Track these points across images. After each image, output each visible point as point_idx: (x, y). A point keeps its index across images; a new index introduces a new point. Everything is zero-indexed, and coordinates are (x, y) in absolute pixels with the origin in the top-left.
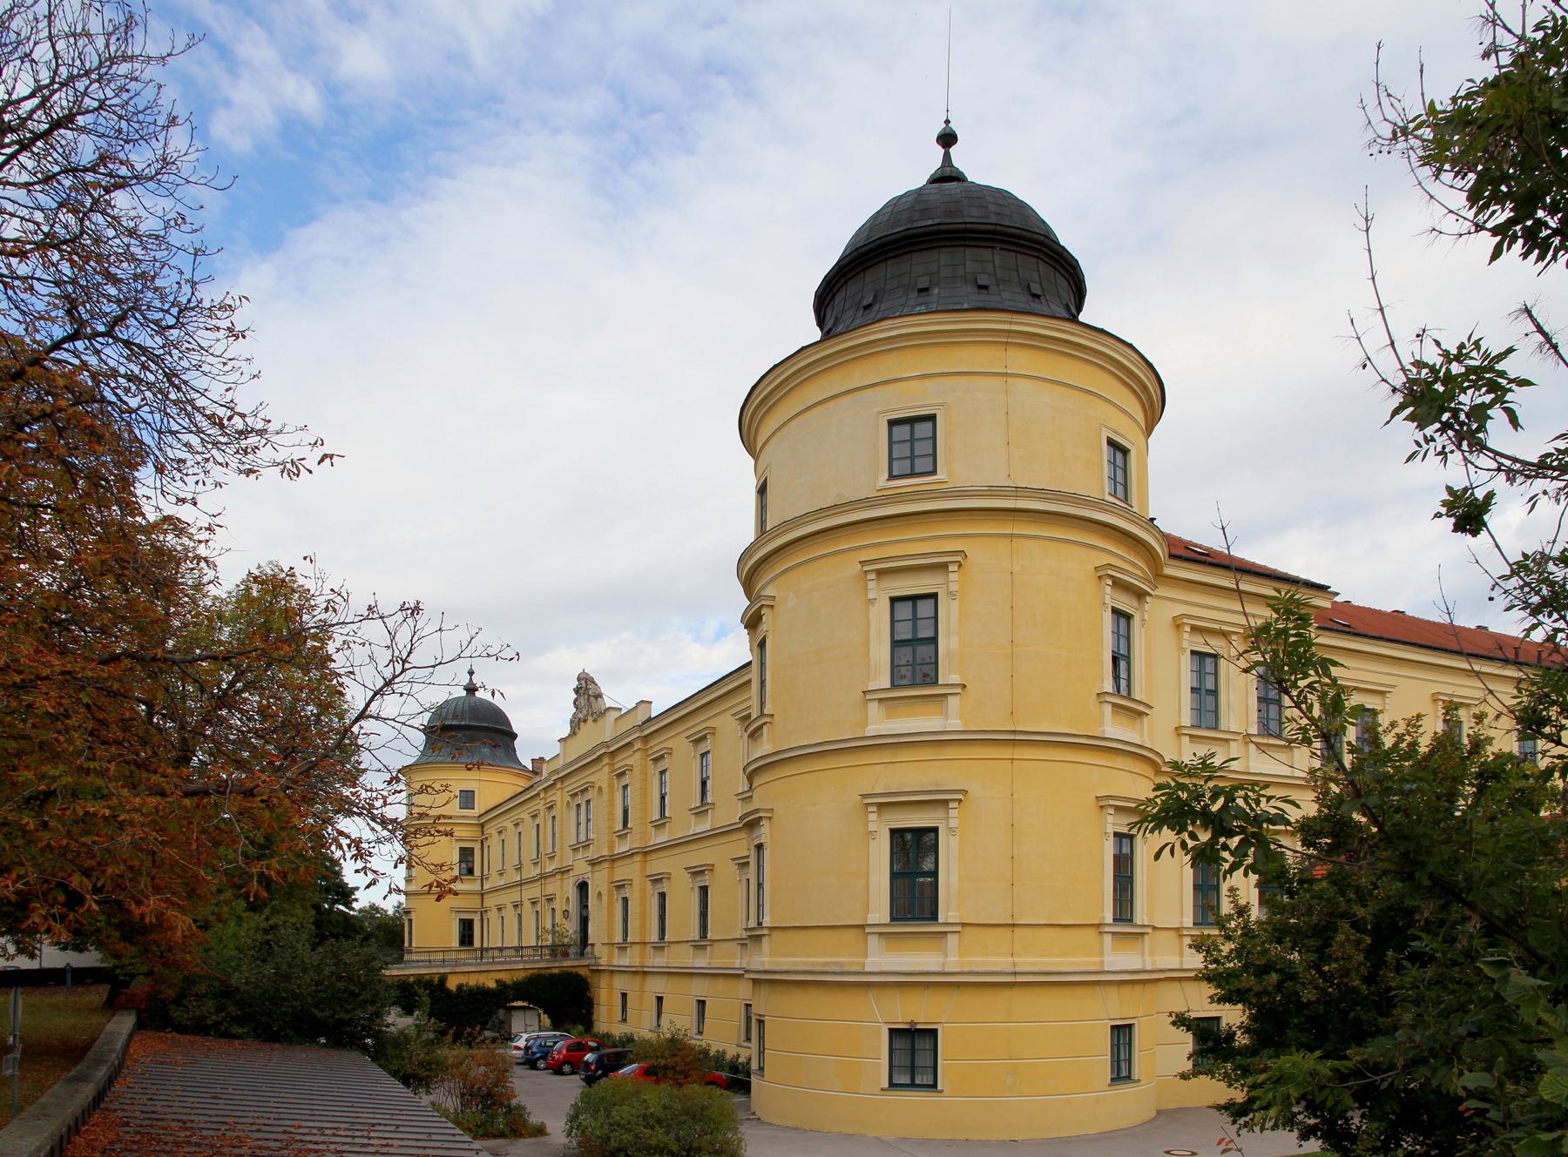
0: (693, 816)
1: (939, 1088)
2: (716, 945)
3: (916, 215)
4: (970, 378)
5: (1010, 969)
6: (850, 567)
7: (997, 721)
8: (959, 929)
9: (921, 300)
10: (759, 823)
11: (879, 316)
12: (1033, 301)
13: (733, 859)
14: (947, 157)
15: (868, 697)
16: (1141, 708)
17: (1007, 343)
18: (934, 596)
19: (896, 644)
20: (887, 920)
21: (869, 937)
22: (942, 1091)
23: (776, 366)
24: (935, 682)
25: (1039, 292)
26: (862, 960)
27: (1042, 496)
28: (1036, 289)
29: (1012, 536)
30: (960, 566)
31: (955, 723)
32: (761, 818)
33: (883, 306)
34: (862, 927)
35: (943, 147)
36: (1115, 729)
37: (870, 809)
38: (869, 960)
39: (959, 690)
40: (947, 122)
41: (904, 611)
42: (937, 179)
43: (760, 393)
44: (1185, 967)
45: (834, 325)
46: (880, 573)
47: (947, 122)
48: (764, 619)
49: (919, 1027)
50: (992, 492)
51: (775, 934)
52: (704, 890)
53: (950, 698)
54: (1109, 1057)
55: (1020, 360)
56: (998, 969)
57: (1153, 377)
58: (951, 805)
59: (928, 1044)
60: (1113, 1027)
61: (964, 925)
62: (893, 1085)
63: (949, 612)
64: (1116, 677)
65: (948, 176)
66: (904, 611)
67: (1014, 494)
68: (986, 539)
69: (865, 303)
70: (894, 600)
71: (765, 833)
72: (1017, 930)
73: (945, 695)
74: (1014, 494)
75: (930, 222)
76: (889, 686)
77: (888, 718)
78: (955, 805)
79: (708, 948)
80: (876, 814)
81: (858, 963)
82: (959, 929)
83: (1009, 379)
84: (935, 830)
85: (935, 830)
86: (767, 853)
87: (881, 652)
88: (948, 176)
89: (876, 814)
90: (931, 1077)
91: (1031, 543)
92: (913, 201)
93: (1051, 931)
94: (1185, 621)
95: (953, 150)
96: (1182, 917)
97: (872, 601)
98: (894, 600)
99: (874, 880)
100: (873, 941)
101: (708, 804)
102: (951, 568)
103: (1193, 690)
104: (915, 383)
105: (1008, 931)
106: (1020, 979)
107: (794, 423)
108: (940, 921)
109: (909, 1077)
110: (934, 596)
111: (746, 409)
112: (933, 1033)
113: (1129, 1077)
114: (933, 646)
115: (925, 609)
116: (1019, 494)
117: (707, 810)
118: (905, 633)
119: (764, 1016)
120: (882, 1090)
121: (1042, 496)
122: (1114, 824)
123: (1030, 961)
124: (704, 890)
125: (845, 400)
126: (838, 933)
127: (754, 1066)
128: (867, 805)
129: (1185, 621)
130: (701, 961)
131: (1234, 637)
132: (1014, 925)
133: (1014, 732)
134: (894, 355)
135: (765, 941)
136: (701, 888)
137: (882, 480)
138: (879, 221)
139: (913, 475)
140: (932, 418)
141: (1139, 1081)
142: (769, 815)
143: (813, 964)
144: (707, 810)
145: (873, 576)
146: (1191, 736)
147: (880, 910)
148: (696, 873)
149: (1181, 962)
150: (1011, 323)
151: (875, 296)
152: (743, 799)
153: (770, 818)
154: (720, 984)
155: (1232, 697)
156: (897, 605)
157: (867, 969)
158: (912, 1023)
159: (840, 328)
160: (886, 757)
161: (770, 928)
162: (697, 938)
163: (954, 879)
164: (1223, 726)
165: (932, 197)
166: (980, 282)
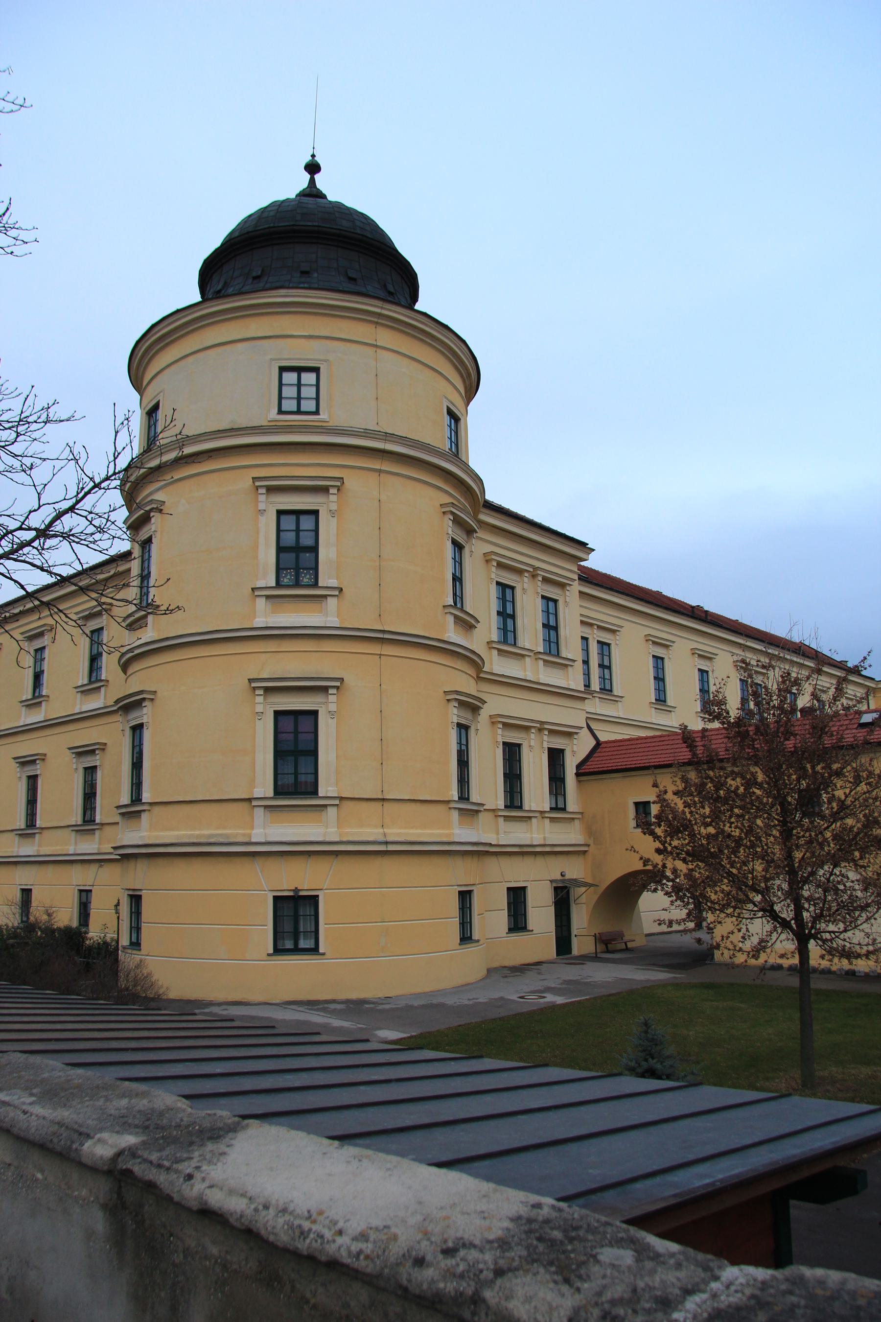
0: (24, 708)
1: (321, 951)
2: (45, 832)
3: (298, 217)
4: (348, 344)
5: (381, 839)
6: (244, 481)
7: (367, 621)
8: (337, 802)
9: (303, 279)
10: (141, 704)
11: (268, 286)
12: (390, 297)
13: (70, 749)
14: (312, 182)
15: (257, 593)
16: (473, 622)
17: (377, 323)
18: (316, 513)
19: (281, 550)
20: (270, 793)
21: (256, 809)
22: (324, 954)
23: (178, 311)
24: (315, 585)
25: (392, 290)
26: (248, 831)
27: (404, 442)
28: (391, 288)
29: (380, 471)
30: (338, 490)
31: (333, 620)
32: (144, 699)
33: (271, 279)
34: (249, 800)
35: (309, 173)
36: (453, 634)
37: (257, 692)
38: (255, 831)
39: (337, 593)
40: (313, 156)
41: (289, 523)
42: (302, 194)
43: (159, 331)
44: (500, 843)
45: (223, 287)
46: (271, 490)
47: (313, 156)
48: (153, 520)
49: (302, 893)
50: (367, 433)
51: (157, 809)
52: (33, 780)
53: (329, 598)
54: (458, 919)
55: (385, 337)
56: (371, 839)
57: (473, 365)
58: (331, 691)
59: (309, 911)
60: (460, 892)
61: (341, 799)
62: (278, 950)
63: (328, 528)
64: (455, 595)
65: (312, 193)
66: (289, 523)
67: (384, 438)
68: (357, 471)
69: (254, 274)
70: (280, 513)
71: (146, 714)
72: (386, 804)
73: (325, 596)
74: (384, 438)
75: (310, 224)
76: (274, 585)
77: (272, 613)
78: (334, 691)
79: (37, 836)
80: (262, 697)
81: (244, 835)
82: (337, 802)
83: (378, 350)
84: (315, 713)
85: (315, 713)
86: (147, 734)
87: (268, 555)
88: (312, 193)
89: (262, 697)
90: (313, 941)
91: (394, 479)
92: (278, 209)
93: (413, 805)
94: (493, 557)
95: (317, 177)
96: (497, 800)
97: (262, 512)
98: (280, 513)
99: (259, 757)
100: (259, 813)
101: (102, 681)
102: (332, 491)
103: (499, 613)
104: (303, 341)
105: (379, 804)
106: (391, 848)
107: (190, 359)
108: (320, 795)
109: (292, 942)
110: (316, 513)
111: (141, 344)
112: (313, 900)
113: (470, 938)
114: (313, 555)
115: (306, 523)
116: (387, 438)
117: (41, 702)
118: (289, 539)
119: (141, 890)
120: (269, 955)
121: (404, 442)
122: (458, 716)
123: (398, 832)
124: (33, 780)
125: (240, 346)
126: (224, 805)
127: (124, 941)
128: (254, 688)
129: (493, 557)
130: (28, 849)
131: (526, 574)
132: (384, 800)
133: (383, 632)
134: (287, 317)
135: (144, 816)
136: (29, 777)
137: (273, 414)
138: (265, 215)
139: (299, 412)
140: (316, 370)
141: (478, 941)
142: (152, 697)
143: (198, 836)
144: (41, 702)
145: (264, 491)
146: (499, 650)
147: (265, 787)
148: (25, 762)
149: (498, 839)
150: (382, 308)
151: (263, 271)
152: (82, 692)
153: (152, 700)
154: (50, 872)
155: (526, 621)
156: (283, 518)
157: (253, 840)
158: (296, 890)
159: (230, 291)
160: (271, 646)
161: (151, 804)
162: (23, 826)
163: (332, 757)
164: (520, 643)
165: (310, 206)
166: (350, 275)
